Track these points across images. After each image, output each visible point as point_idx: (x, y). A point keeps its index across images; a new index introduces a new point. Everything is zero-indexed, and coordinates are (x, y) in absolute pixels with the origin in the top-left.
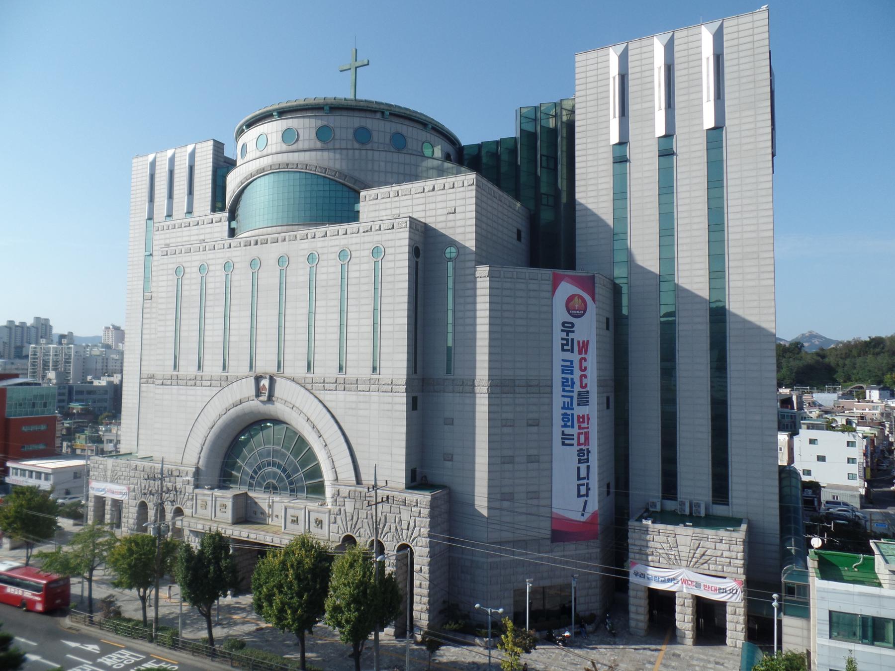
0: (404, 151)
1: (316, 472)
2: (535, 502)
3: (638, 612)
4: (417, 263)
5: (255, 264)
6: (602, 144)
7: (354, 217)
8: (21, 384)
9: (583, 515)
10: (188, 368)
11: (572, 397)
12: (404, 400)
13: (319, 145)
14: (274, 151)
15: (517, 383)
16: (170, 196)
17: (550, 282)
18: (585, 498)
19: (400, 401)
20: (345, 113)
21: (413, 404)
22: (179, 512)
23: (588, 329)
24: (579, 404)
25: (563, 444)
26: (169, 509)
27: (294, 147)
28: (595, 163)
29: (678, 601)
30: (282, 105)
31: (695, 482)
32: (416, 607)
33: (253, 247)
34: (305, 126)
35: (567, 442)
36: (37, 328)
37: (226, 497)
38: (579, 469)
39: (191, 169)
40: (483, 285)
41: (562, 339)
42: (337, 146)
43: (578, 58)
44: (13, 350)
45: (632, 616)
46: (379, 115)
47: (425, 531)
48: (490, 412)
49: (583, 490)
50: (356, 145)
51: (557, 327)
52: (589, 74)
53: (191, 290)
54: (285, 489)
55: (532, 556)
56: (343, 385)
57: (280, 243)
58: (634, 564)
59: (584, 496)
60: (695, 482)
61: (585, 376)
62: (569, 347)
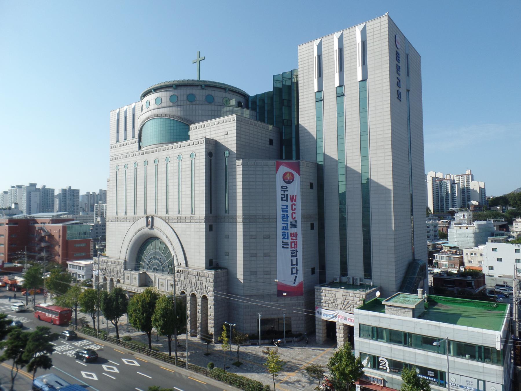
0: (213, 104)
1: (172, 263)
2: (268, 276)
3: (321, 333)
4: (211, 160)
5: (145, 163)
6: (311, 92)
7: (187, 138)
8: (75, 224)
9: (294, 283)
10: (121, 214)
11: (287, 224)
12: (204, 226)
13: (171, 104)
14: (152, 108)
15: (257, 217)
16: (126, 129)
17: (275, 166)
18: (295, 275)
19: (203, 226)
20: (183, 88)
21: (210, 228)
22: (118, 281)
23: (295, 188)
24: (291, 228)
25: (283, 247)
26: (115, 280)
27: (160, 106)
28: (308, 102)
29: (337, 327)
30: (155, 86)
31: (356, 268)
32: (210, 325)
33: (145, 155)
34: (165, 95)
35: (285, 246)
36: (88, 196)
37: (136, 274)
38: (292, 260)
39: (134, 115)
40: (239, 170)
41: (282, 195)
42: (179, 104)
43: (299, 48)
44: (89, 207)
45: (317, 334)
46: (199, 87)
47: (212, 289)
48: (243, 232)
49: (294, 271)
50: (188, 103)
51: (279, 189)
52: (304, 56)
53: (122, 177)
54: (161, 270)
55: (259, 303)
56: (180, 220)
57: (155, 153)
58: (317, 308)
59: (294, 274)
60: (356, 268)
61: (295, 213)
62: (285, 199)
